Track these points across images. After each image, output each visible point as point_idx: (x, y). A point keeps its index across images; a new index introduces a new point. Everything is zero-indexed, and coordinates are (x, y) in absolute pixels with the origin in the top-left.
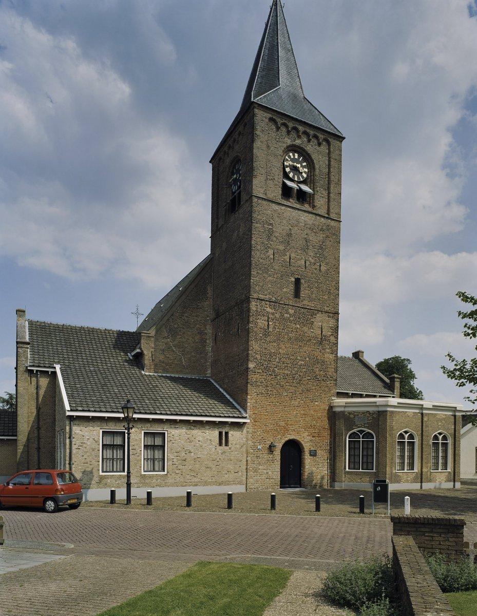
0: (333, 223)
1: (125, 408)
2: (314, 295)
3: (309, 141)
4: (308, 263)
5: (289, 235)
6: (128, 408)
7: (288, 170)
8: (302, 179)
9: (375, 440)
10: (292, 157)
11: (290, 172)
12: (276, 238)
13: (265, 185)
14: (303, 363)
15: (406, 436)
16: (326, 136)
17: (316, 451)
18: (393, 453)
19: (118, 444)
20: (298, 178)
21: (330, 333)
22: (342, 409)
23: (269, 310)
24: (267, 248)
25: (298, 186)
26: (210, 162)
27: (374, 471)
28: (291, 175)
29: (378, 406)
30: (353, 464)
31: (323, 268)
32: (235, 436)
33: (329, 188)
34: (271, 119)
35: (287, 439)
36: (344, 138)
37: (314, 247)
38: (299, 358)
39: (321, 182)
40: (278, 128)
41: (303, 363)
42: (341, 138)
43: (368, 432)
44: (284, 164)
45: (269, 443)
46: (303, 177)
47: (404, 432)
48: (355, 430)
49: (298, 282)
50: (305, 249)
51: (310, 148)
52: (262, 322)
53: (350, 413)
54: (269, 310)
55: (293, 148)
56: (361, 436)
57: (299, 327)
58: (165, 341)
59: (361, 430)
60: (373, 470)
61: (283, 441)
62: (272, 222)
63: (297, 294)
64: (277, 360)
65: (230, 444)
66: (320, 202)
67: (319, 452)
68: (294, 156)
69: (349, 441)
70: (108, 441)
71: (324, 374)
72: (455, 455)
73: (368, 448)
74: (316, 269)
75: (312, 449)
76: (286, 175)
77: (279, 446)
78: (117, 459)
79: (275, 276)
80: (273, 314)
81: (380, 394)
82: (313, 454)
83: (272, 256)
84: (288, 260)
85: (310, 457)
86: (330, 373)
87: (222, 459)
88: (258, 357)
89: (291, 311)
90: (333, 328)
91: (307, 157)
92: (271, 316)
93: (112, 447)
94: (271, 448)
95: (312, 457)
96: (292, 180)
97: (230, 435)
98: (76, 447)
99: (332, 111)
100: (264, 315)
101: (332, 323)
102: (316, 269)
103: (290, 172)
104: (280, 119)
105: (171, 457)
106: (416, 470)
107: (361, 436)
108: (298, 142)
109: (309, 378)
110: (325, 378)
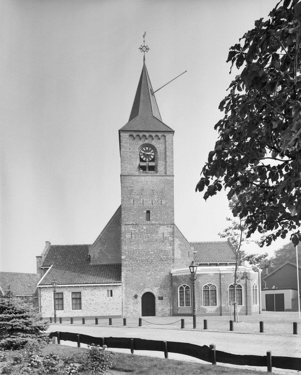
0: (168, 178)
1: (192, 267)
2: (158, 218)
3: (153, 139)
4: (154, 202)
5: (142, 190)
6: (193, 267)
7: (142, 157)
8: (150, 159)
10: (145, 150)
11: (143, 158)
12: (135, 193)
14: (153, 253)
15: (184, 288)
16: (162, 134)
17: (162, 297)
18: (200, 298)
20: (149, 159)
21: (169, 235)
23: (132, 229)
24: (129, 199)
30: (182, 304)
31: (163, 203)
32: (116, 292)
33: (166, 160)
34: (131, 135)
35: (145, 292)
37: (157, 193)
38: (150, 250)
40: (134, 139)
41: (153, 253)
42: (172, 132)
44: (140, 154)
45: (135, 294)
46: (151, 158)
47: (183, 286)
48: (206, 284)
49: (148, 212)
50: (152, 195)
51: (153, 143)
52: (128, 236)
53: (179, 277)
54: (132, 229)
56: (210, 287)
57: (150, 235)
58: (100, 248)
61: (143, 293)
62: (132, 185)
63: (148, 219)
64: (138, 253)
65: (113, 296)
66: (160, 168)
67: (164, 298)
68: (146, 149)
70: (74, 296)
71: (166, 257)
72: (246, 296)
73: (58, 304)
74: (159, 204)
75: (160, 296)
78: (78, 304)
79: (135, 212)
80: (134, 231)
81: (230, 262)
82: (161, 298)
83: (132, 203)
84: (142, 202)
85: (159, 300)
86: (170, 257)
87: (109, 303)
88: (127, 253)
89: (145, 228)
90: (171, 233)
91: (153, 148)
92: (133, 232)
93: (76, 299)
94: (136, 297)
95: (160, 300)
97: (113, 291)
98: (43, 300)
100: (129, 232)
101: (170, 230)
102: (159, 204)
103: (143, 158)
105: (51, 307)
106: (218, 306)
108: (147, 142)
109: (157, 260)
110: (166, 259)
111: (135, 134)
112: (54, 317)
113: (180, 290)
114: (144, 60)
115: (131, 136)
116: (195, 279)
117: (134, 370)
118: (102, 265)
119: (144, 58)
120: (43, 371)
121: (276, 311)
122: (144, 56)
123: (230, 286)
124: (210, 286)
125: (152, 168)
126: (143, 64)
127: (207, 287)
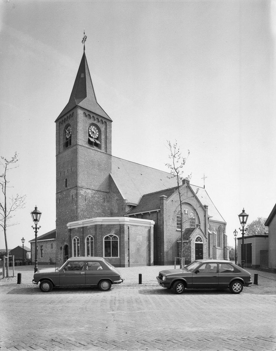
7: (90, 133)
9: (118, 240)
13: (81, 139)
16: (106, 120)
19: (235, 262)
20: (95, 137)
22: (100, 223)
25: (94, 140)
26: (56, 121)
27: (119, 257)
28: (92, 135)
29: (120, 222)
36: (112, 121)
39: (103, 137)
43: (115, 236)
44: (89, 131)
46: (96, 136)
48: (108, 235)
51: (99, 124)
55: (93, 124)
56: (111, 238)
59: (111, 235)
60: (118, 256)
66: (103, 146)
69: (105, 241)
76: (90, 136)
77: (63, 247)
96: (92, 138)
99: (110, 112)
104: (89, 114)
107: (111, 238)
108: (96, 122)
111: (87, 113)
112: (6, 249)
113: (105, 240)
114: (84, 49)
115: (84, 113)
116: (39, 228)
117: (252, 292)
118: (163, 222)
119: (84, 48)
120: (122, 291)
121: (95, 256)
122: (84, 46)
123: (105, 238)
124: (111, 237)
125: (96, 145)
126: (83, 53)
127: (116, 238)
